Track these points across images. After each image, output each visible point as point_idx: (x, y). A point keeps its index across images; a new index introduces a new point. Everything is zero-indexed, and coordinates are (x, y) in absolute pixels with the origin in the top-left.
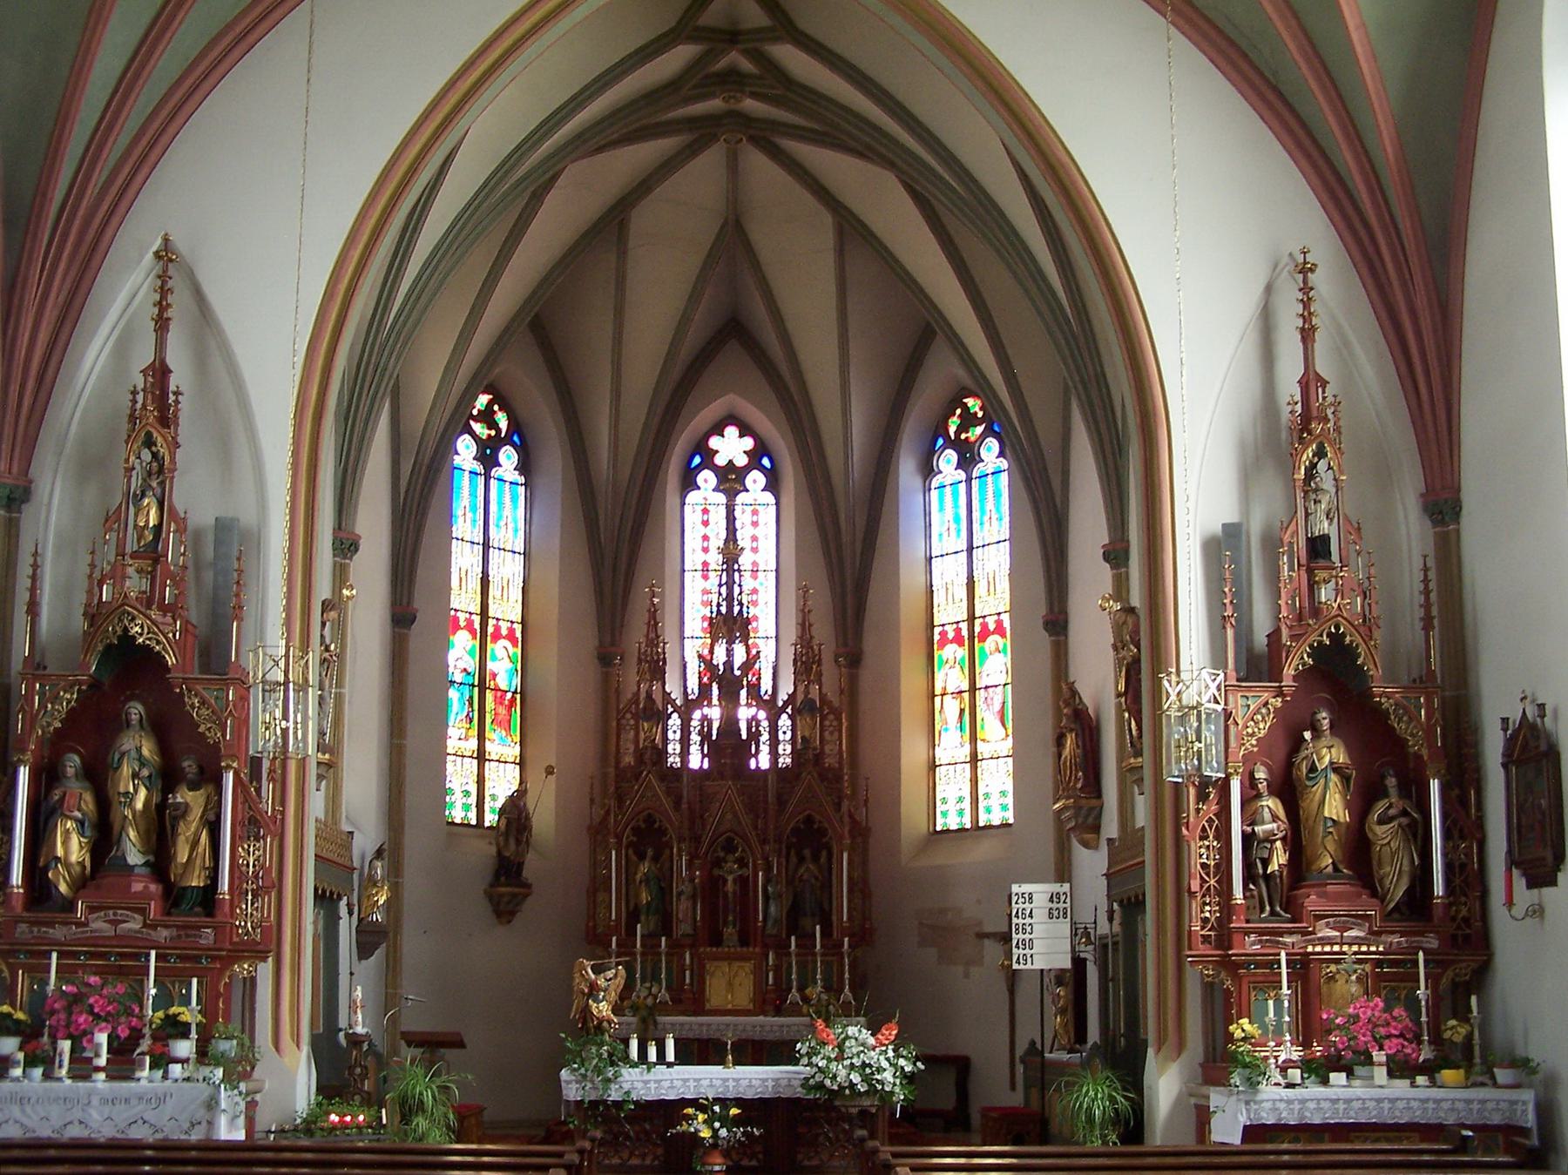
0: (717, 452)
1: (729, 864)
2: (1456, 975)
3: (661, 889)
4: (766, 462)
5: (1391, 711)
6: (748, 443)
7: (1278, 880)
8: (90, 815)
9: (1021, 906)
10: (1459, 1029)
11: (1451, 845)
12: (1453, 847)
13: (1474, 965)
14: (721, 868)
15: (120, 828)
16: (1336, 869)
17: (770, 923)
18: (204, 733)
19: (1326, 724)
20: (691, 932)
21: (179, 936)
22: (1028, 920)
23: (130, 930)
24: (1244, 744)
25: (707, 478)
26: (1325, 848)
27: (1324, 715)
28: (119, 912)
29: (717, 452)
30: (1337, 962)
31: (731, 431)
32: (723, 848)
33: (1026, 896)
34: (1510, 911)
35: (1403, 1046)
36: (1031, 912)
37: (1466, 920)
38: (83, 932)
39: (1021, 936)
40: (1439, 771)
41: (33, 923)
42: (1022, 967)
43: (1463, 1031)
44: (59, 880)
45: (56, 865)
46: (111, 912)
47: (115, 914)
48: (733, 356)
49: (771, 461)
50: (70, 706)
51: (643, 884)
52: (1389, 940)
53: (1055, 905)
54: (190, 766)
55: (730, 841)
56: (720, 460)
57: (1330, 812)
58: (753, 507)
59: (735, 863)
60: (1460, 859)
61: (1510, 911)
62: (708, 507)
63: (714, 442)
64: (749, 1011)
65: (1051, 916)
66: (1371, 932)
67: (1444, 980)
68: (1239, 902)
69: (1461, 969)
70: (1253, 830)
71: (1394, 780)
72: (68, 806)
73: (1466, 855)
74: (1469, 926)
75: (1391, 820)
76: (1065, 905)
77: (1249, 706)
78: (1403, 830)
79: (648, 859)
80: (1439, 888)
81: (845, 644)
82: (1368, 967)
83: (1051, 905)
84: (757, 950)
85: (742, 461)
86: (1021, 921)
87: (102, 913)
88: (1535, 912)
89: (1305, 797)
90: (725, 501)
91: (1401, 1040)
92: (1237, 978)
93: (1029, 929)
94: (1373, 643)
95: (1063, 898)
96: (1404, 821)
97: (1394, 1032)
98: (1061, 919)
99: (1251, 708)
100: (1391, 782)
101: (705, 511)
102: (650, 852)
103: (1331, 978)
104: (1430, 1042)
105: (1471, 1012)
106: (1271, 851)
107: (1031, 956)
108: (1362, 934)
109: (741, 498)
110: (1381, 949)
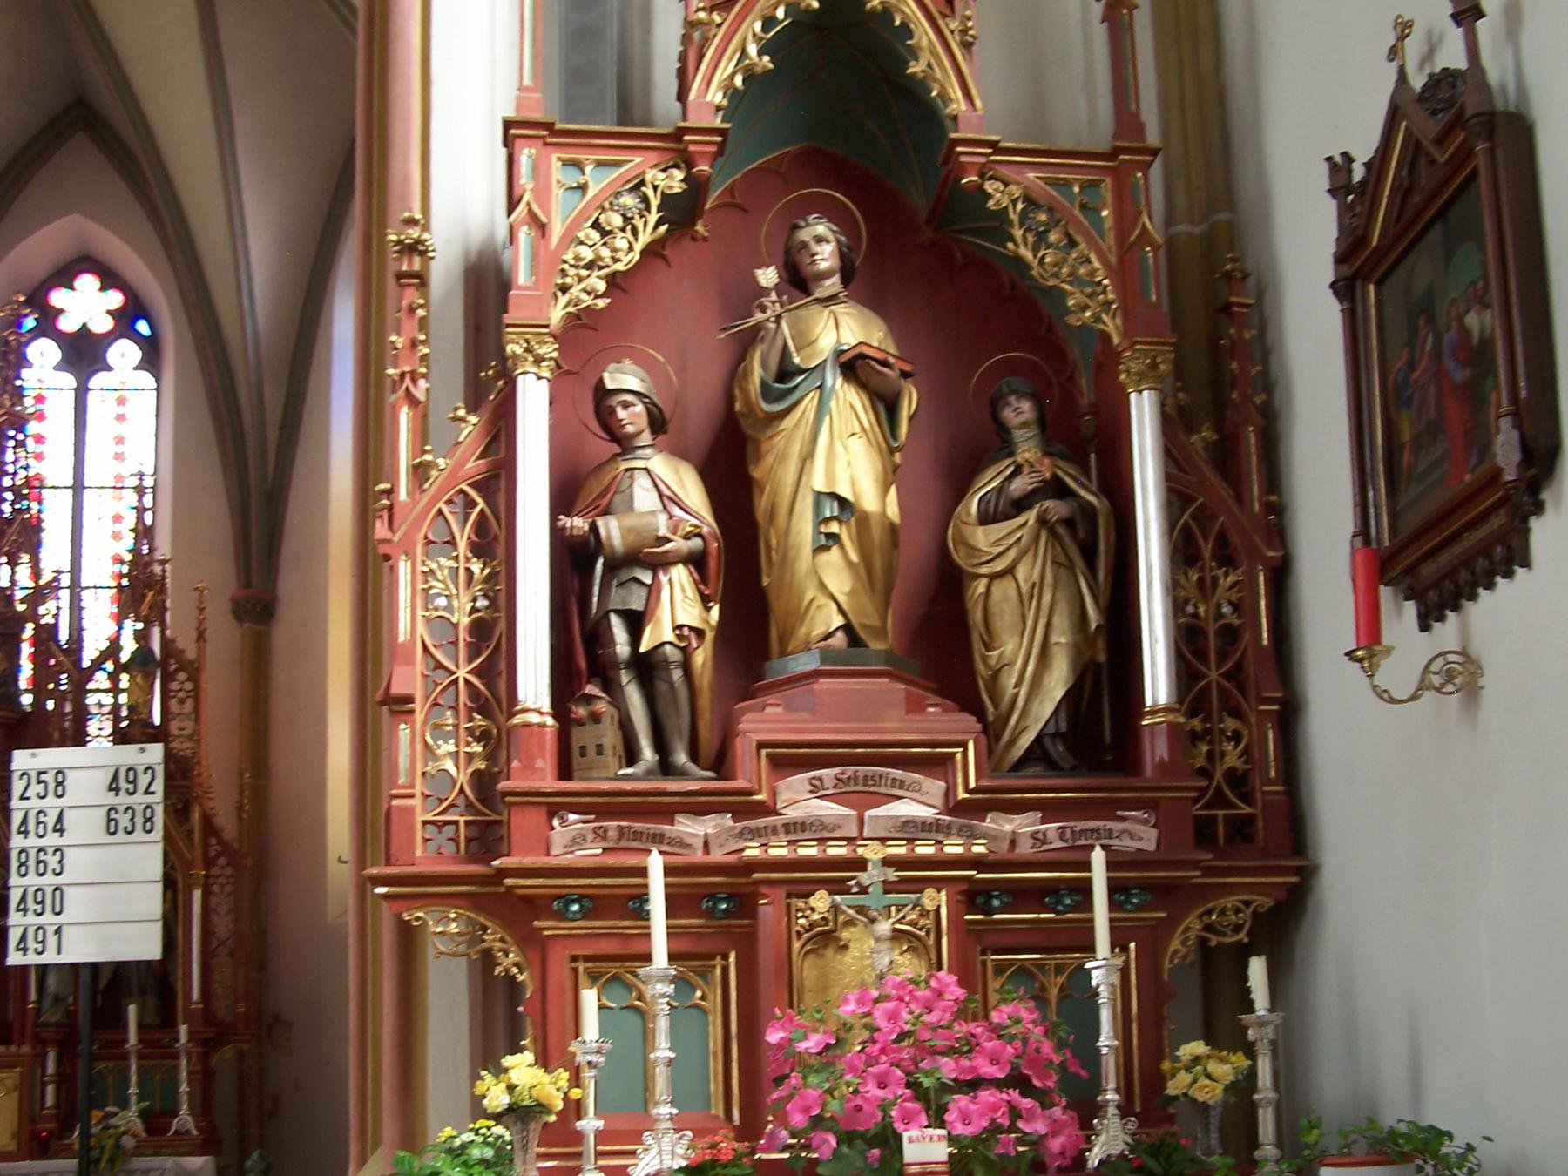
2: (1209, 928)
4: (143, 327)
5: (1013, 216)
6: (115, 299)
7: (677, 674)
9: (35, 803)
10: (1215, 1068)
11: (1195, 577)
12: (1201, 580)
13: (1264, 902)
16: (854, 639)
17: (47, 1003)
19: (826, 256)
22: (52, 840)
24: (564, 289)
26: (822, 586)
27: (821, 229)
29: (61, 311)
30: (838, 887)
31: (87, 283)
33: (49, 778)
34: (1370, 673)
35: (1015, 1113)
36: (60, 819)
37: (1237, 780)
39: (32, 880)
40: (1154, 366)
42: (32, 959)
43: (1225, 1069)
49: (152, 327)
52: (1008, 828)
53: (123, 800)
56: (68, 324)
57: (830, 474)
58: (119, 393)
60: (1219, 616)
61: (1370, 673)
62: (44, 393)
63: (58, 298)
64: (10, 1153)
65: (111, 827)
66: (956, 808)
67: (1175, 944)
68: (534, 718)
69: (1223, 912)
70: (594, 528)
71: (1026, 406)
73: (1236, 606)
74: (1247, 798)
75: (1020, 505)
76: (149, 799)
77: (582, 188)
78: (1052, 532)
80: (1158, 685)
81: (248, 583)
82: (937, 900)
83: (111, 799)
84: (26, 1049)
85: (102, 325)
86: (32, 842)
88: (1450, 676)
89: (764, 447)
90: (74, 385)
91: (1014, 1094)
92: (535, 945)
93: (53, 862)
94: (954, 25)
95: (143, 781)
96: (1056, 508)
97: (988, 1070)
98: (139, 835)
99: (591, 193)
100: (1019, 412)
103: (826, 938)
104: (1125, 1110)
105: (1249, 1007)
106: (653, 590)
107: (58, 931)
108: (925, 812)
109: (98, 380)
110: (979, 849)
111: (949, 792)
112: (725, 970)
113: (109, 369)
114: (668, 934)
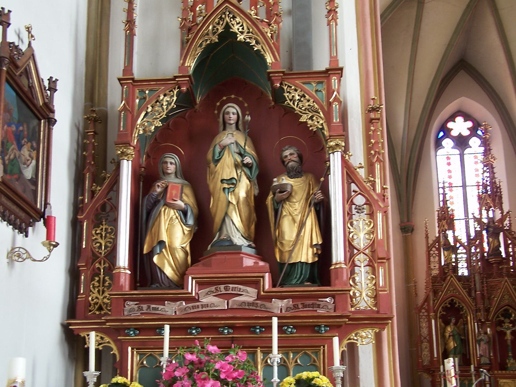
0: (452, 129)
1: (506, 324)
3: (462, 340)
6: (470, 124)
8: (191, 204)
14: (502, 326)
15: (220, 223)
18: (306, 123)
20: (488, 362)
21: (295, 307)
23: (244, 303)
25: (448, 143)
28: (231, 286)
29: (452, 129)
31: (459, 120)
32: (503, 315)
38: (193, 307)
41: (141, 301)
44: (164, 264)
45: (161, 251)
46: (222, 287)
47: (226, 289)
48: (463, 78)
50: (170, 108)
51: (451, 338)
54: (291, 154)
55: (506, 310)
56: (454, 133)
59: (510, 323)
62: (449, 156)
63: (450, 125)
72: (171, 194)
79: (452, 324)
87: (213, 288)
101: (448, 158)
102: (453, 320)
109: (467, 151)
111: (259, 293)
112: (324, 350)
113: (471, 147)
114: (170, 341)
